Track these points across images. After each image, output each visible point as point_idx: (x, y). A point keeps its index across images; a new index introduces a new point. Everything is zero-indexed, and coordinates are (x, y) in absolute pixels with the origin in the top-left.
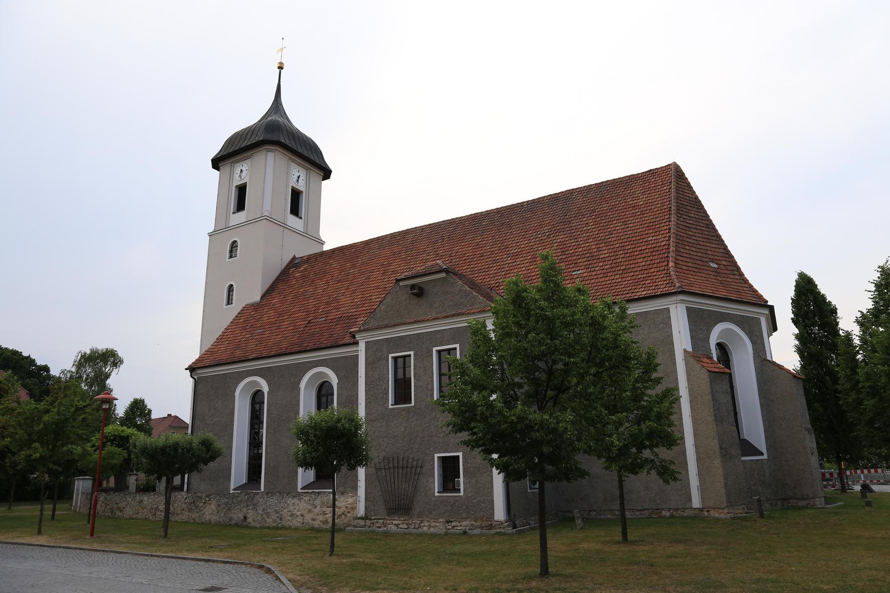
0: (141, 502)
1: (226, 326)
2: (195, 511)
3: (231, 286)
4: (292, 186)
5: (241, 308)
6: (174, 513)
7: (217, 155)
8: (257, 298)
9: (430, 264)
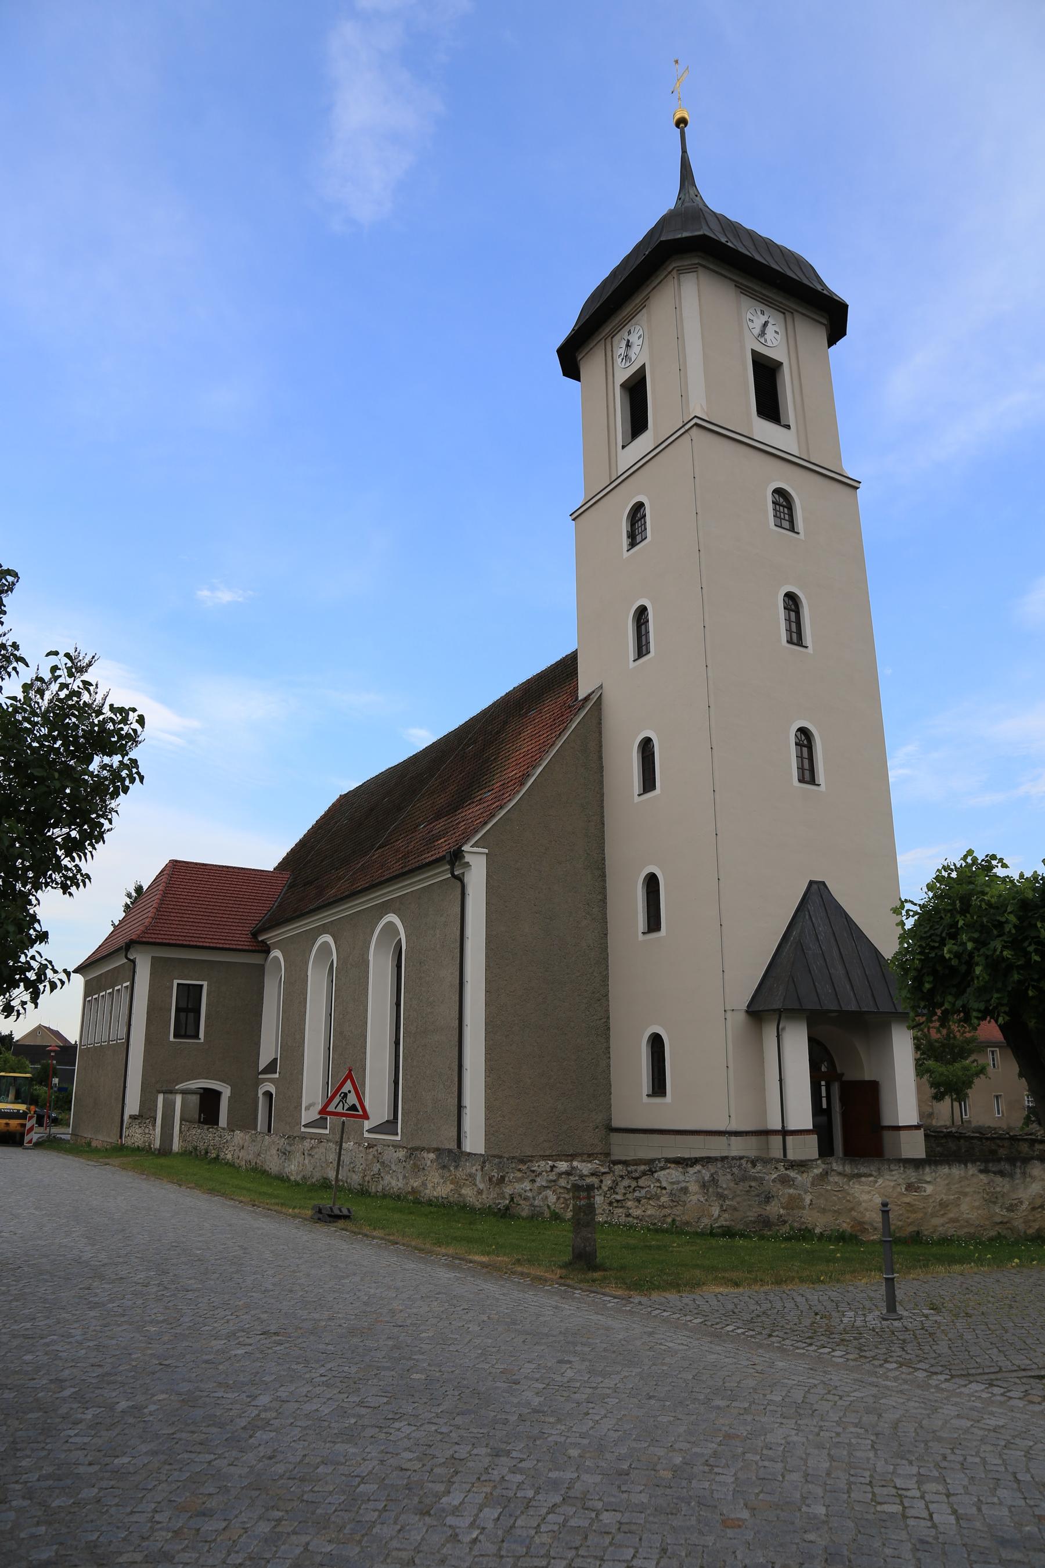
3: (640, 506)
4: (753, 352)
7: (573, 330)
9: (447, 1276)
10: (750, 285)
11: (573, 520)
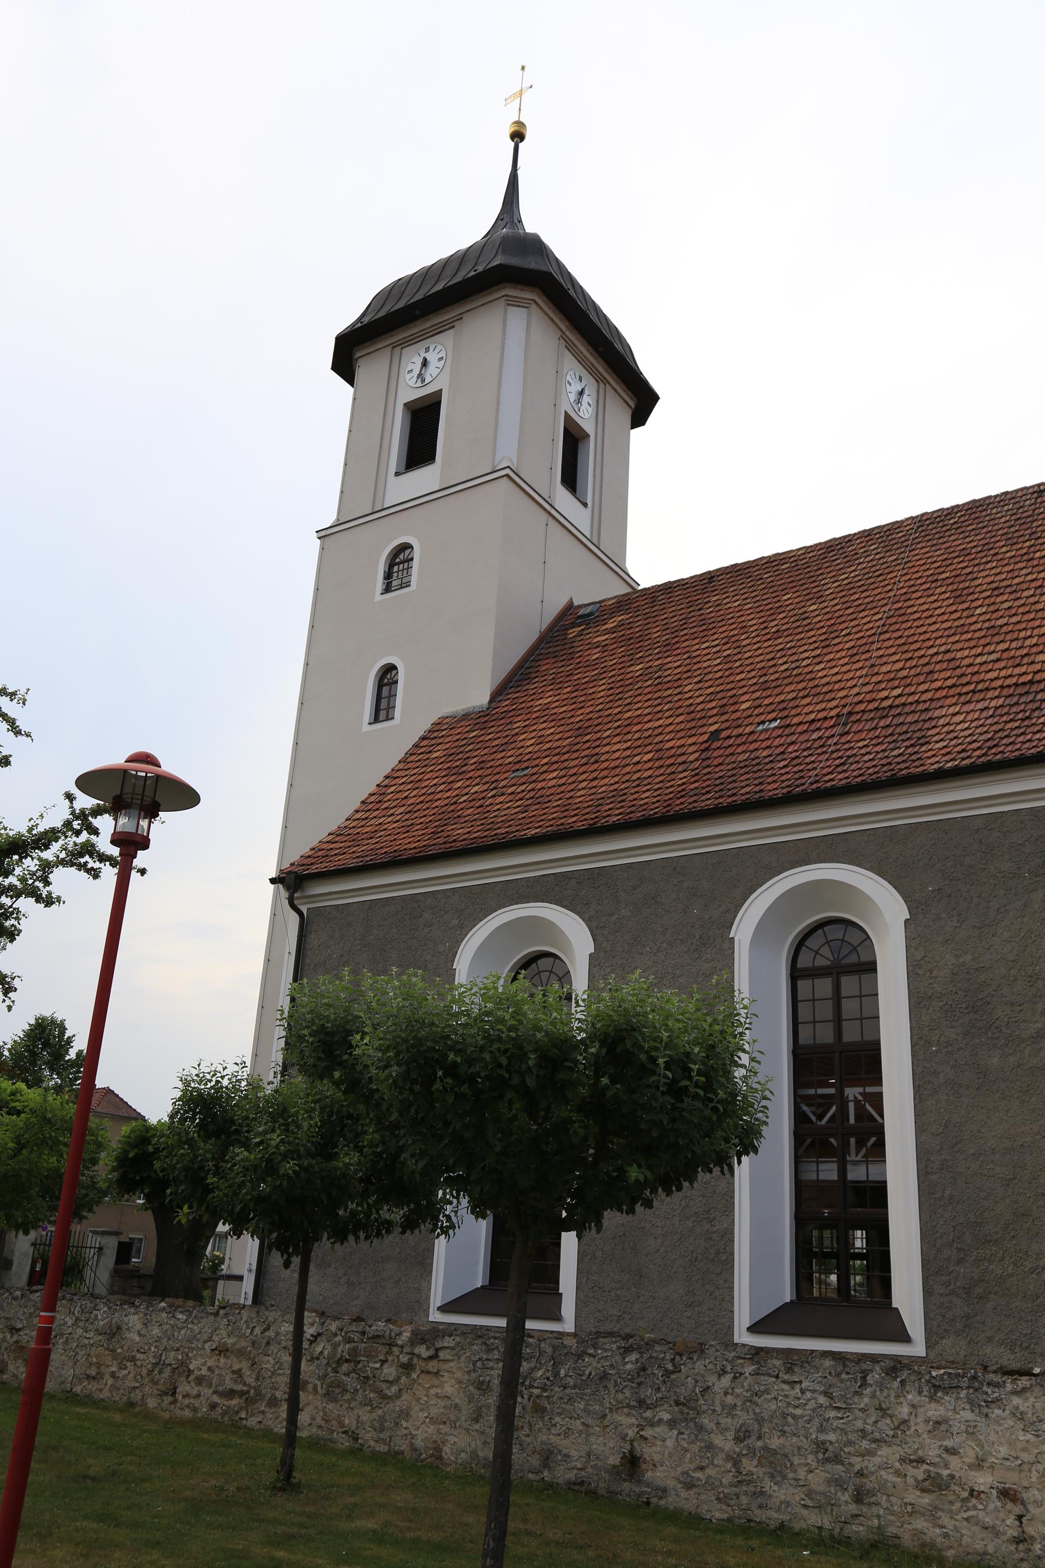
0: (114, 1332)
1: (387, 771)
2: (359, 1397)
5: (428, 726)
6: (258, 1393)
8: (479, 697)
10: (596, 364)
11: (319, 538)
